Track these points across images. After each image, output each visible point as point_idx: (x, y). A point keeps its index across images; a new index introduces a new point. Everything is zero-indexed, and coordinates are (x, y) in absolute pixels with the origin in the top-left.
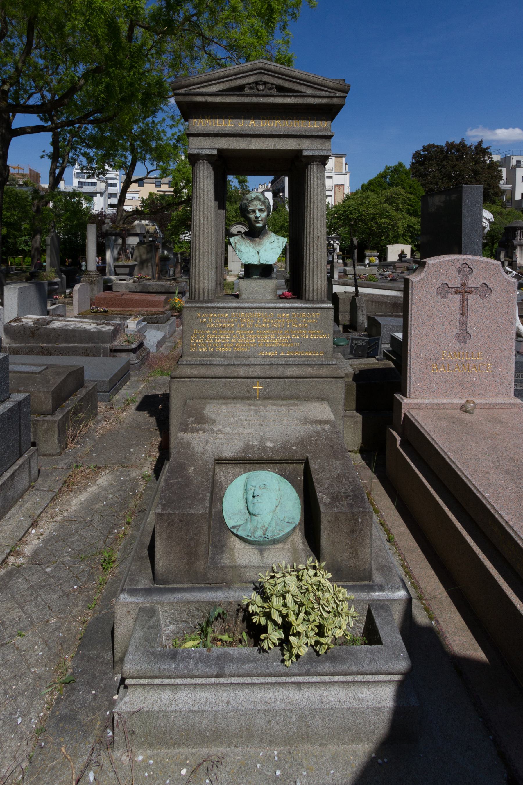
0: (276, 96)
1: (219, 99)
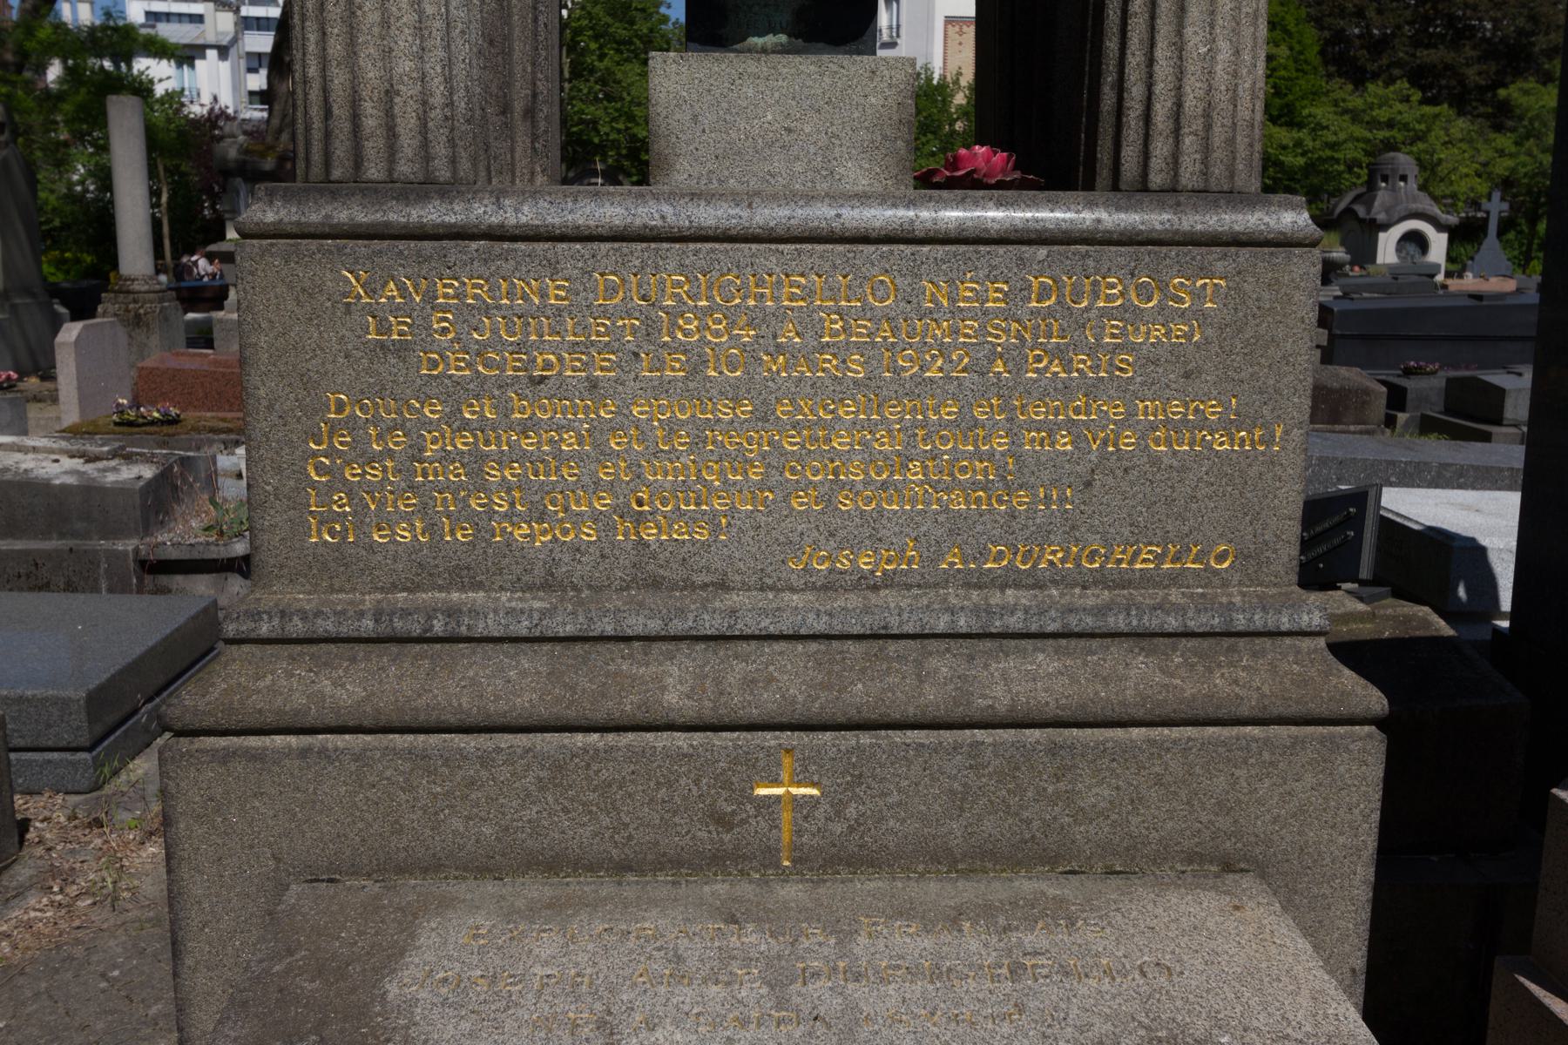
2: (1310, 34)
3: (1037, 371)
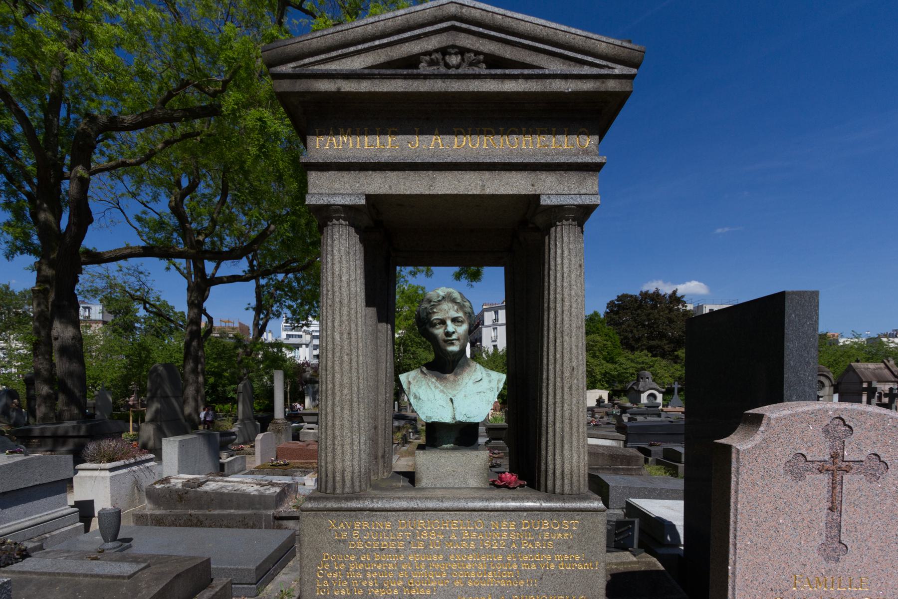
1: (365, 86)
2: (617, 337)
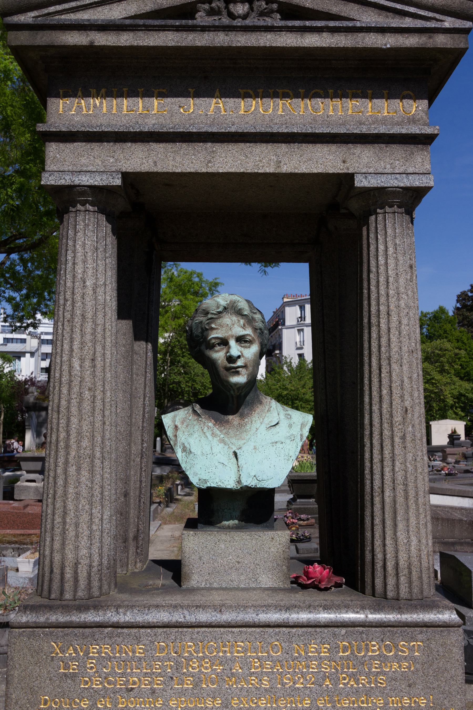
0: (280, 29)
1: (125, 39)
3: (344, 684)
